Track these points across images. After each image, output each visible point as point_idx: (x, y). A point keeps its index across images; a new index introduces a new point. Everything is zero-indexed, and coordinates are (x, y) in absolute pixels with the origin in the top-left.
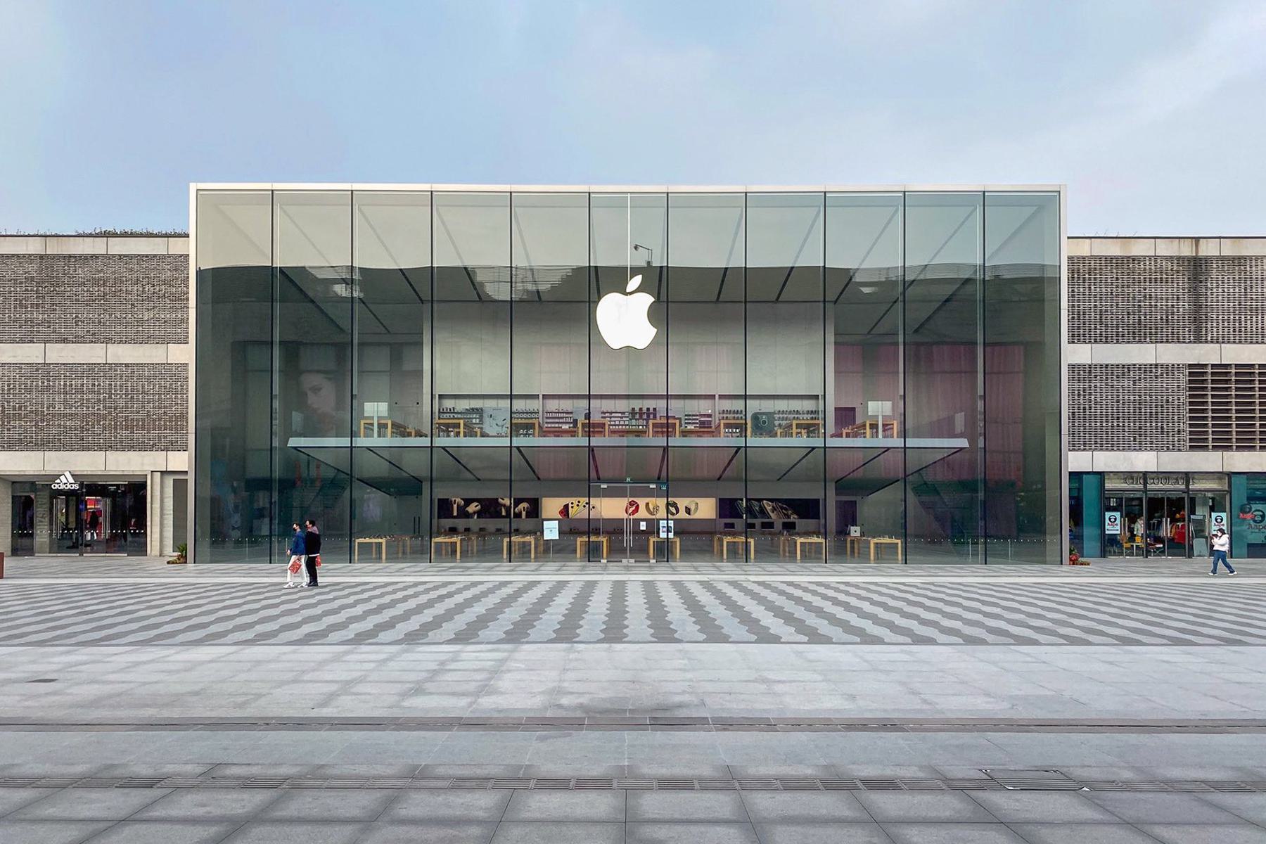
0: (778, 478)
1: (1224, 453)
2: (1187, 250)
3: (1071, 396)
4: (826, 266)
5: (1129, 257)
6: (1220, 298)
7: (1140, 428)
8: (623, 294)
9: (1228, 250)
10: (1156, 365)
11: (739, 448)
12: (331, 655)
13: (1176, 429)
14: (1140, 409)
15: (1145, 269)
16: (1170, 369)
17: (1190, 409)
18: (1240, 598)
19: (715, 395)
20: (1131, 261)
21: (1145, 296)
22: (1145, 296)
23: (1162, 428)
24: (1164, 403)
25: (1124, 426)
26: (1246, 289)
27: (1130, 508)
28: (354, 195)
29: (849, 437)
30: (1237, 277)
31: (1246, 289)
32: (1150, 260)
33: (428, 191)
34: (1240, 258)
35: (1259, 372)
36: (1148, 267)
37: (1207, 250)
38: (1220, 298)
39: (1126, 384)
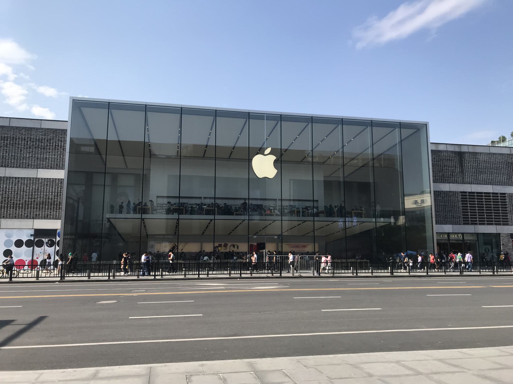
0: (229, 233)
1: (497, 226)
2: (457, 149)
3: (62, 194)
4: (108, 139)
5: (438, 151)
6: (470, 167)
7: (446, 215)
8: (263, 155)
9: (471, 150)
10: (450, 191)
11: (211, 220)
12: (25, 325)
13: (458, 216)
14: (445, 208)
15: (444, 156)
16: (455, 193)
17: (462, 209)
18: (183, 286)
19: (202, 197)
20: (439, 152)
21: (444, 165)
22: (444, 165)
23: (453, 216)
24: (454, 206)
25: (440, 215)
26: (478, 164)
27: (301, 246)
28: (147, 107)
29: (113, 213)
30: (475, 160)
31: (478, 164)
32: (445, 152)
33: (215, 110)
34: (475, 153)
35: (485, 195)
36: (445, 155)
37: (464, 149)
38: (470, 167)
39: (440, 199)
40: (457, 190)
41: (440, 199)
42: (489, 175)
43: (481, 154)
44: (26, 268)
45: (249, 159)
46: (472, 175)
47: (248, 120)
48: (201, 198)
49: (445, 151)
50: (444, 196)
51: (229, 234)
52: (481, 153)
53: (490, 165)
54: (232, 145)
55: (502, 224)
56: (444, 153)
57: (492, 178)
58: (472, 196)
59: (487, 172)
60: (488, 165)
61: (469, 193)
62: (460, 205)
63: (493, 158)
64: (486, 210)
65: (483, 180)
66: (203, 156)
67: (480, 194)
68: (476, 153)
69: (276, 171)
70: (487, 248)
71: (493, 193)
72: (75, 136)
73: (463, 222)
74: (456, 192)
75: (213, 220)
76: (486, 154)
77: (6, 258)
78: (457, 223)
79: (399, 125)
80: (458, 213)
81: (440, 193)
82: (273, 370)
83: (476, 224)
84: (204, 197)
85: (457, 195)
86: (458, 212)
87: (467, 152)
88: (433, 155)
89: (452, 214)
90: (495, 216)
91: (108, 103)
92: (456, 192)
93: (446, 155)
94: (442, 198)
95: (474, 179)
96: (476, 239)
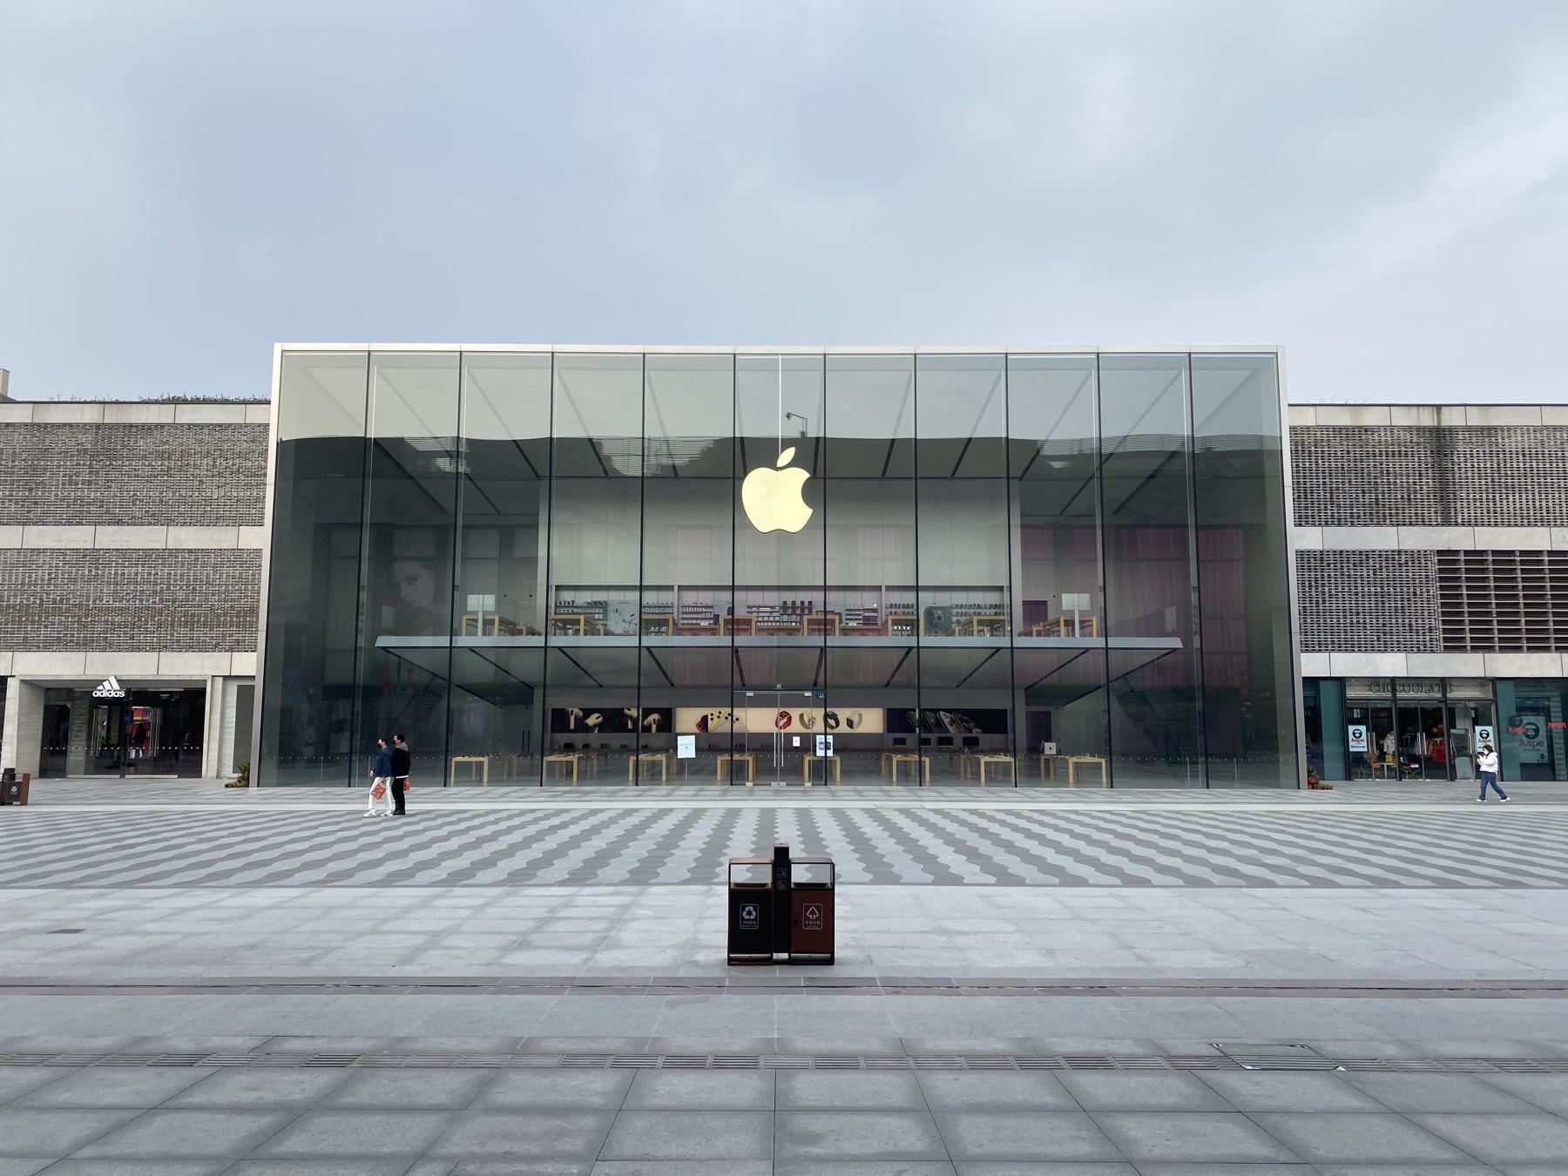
7: (1384, 625)
9: (1475, 419)
11: (910, 649)
13: (1427, 627)
23: (1410, 625)
24: (1411, 596)
32: (1385, 430)
34: (1489, 428)
36: (1383, 439)
37: (1451, 419)
39: (1365, 574)
40: (1422, 547)
41: (1365, 574)
42: (1537, 497)
43: (1506, 432)
44: (36, 787)
45: (734, 478)
46: (1478, 497)
47: (1094, 373)
48: (669, 588)
49: (1385, 428)
50: (1378, 566)
51: (957, 686)
52: (1509, 428)
53: (1541, 465)
54: (968, 436)
55: (1469, 648)
56: (1379, 435)
57: (1551, 504)
58: (1506, 565)
59: (1530, 487)
60: (1534, 465)
61: (1467, 553)
62: (1435, 590)
63: (1552, 443)
64: (1554, 606)
65: (1518, 512)
66: (880, 474)
67: (1503, 557)
68: (1489, 431)
69: (808, 512)
70: (1531, 724)
71: (1550, 553)
72: (289, 436)
73: (1442, 644)
74: (1422, 553)
75: (915, 650)
76: (1528, 430)
77: (980, 736)
78: (1422, 648)
79: (1188, 359)
80: (1426, 616)
81: (1364, 557)
82: (89, 1144)
83: (1490, 649)
84: (556, 586)
85: (1423, 561)
86: (1426, 613)
87: (1463, 427)
88: (1345, 443)
89: (1407, 621)
90: (1556, 623)
91: (1094, 356)
92: (1422, 553)
93: (1389, 439)
94: (1371, 572)
95: (1485, 512)
96: (1491, 697)
